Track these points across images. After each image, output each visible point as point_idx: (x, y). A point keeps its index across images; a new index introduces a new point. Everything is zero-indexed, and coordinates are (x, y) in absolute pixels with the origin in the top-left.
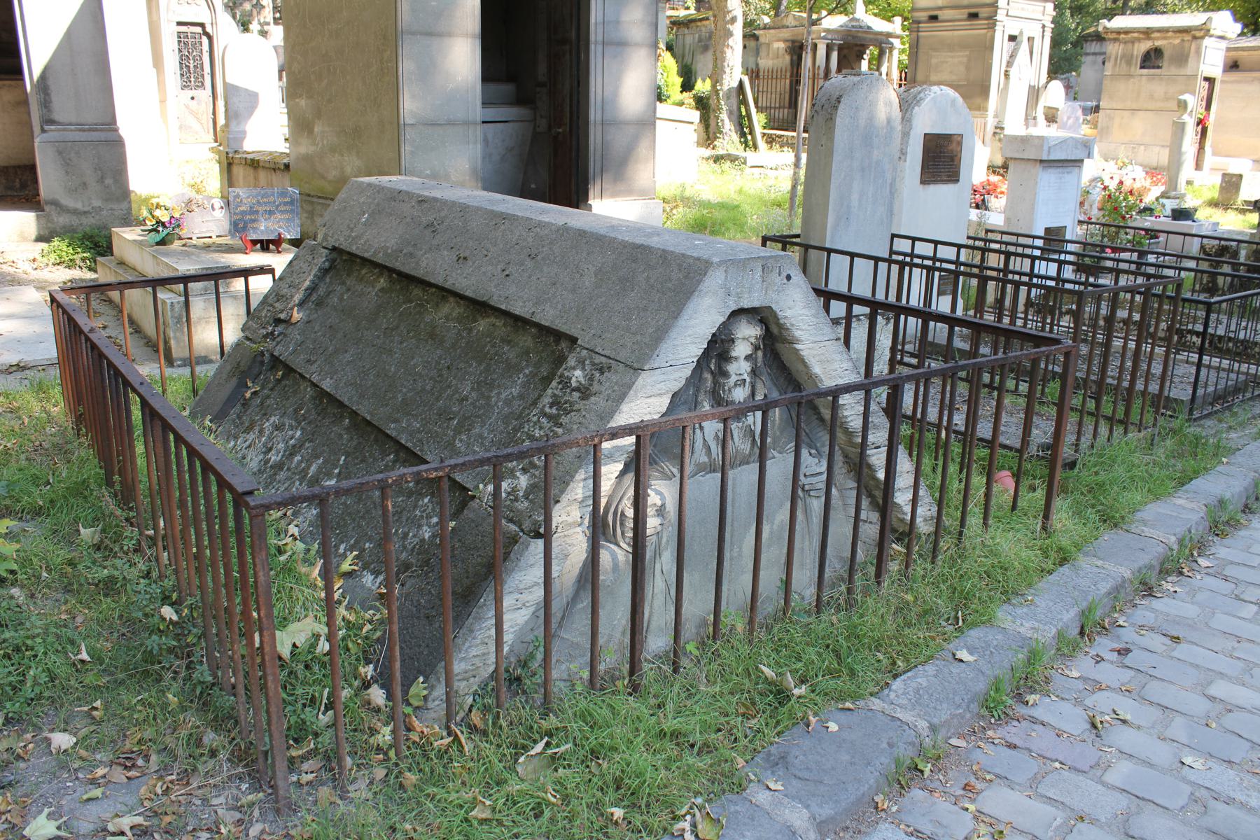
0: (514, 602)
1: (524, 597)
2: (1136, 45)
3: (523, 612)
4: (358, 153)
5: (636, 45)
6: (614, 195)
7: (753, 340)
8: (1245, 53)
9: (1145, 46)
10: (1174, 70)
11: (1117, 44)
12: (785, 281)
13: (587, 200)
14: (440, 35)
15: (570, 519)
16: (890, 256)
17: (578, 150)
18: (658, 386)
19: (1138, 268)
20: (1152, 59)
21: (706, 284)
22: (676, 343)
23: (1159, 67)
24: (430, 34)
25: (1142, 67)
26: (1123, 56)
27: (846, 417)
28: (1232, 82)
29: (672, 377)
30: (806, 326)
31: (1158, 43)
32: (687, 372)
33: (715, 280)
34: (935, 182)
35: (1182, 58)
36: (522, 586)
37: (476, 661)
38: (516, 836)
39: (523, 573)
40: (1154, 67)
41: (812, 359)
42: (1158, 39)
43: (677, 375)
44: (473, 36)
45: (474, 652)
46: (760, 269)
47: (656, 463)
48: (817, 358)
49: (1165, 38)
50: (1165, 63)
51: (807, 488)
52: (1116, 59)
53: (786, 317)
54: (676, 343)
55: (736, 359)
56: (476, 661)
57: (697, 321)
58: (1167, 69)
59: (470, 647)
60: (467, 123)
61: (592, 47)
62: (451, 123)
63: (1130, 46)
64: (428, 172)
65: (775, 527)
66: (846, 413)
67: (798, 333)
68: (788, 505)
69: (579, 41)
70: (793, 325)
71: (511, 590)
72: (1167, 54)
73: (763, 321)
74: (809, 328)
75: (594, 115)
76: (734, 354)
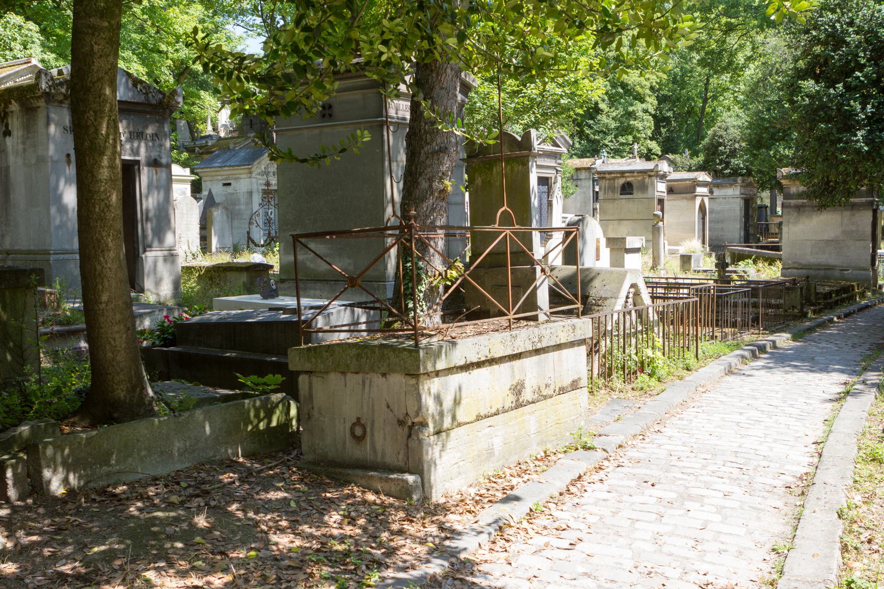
2: (616, 181)
4: (80, 310)
8: (676, 183)
9: (622, 181)
10: (640, 195)
11: (604, 181)
16: (616, 312)
19: (639, 332)
20: (627, 189)
23: (631, 194)
25: (621, 194)
26: (609, 187)
28: (672, 200)
31: (629, 179)
33: (628, 275)
34: (453, 321)
35: (644, 187)
38: (310, 587)
40: (628, 194)
42: (629, 177)
49: (633, 176)
50: (635, 192)
52: (605, 189)
58: (637, 195)
63: (612, 181)
72: (635, 186)
73: (358, 437)
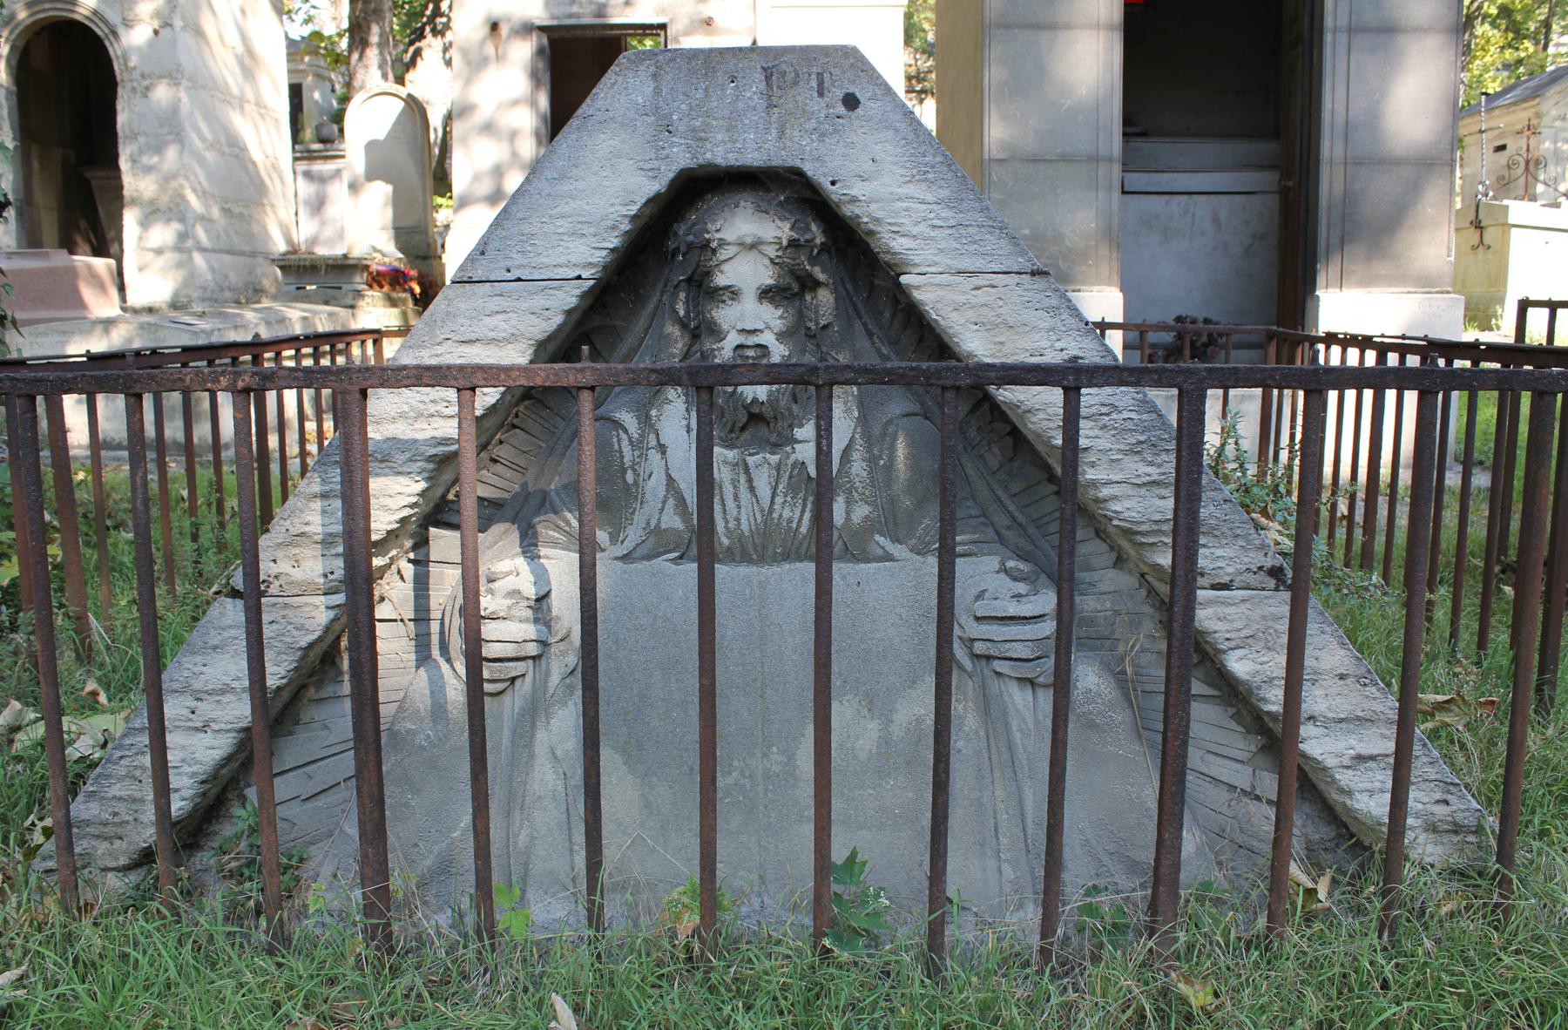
0: (186, 712)
1: (206, 709)
3: (207, 739)
5: (1418, 30)
6: (1368, 282)
7: (772, 251)
12: (841, 109)
13: (1314, 290)
14: (1053, 27)
15: (297, 574)
17: (1307, 211)
18: (487, 320)
21: (600, 103)
22: (526, 229)
24: (1038, 27)
27: (1094, 484)
29: (525, 305)
30: (921, 228)
32: (569, 297)
36: (197, 685)
37: (121, 807)
39: (198, 659)
41: (954, 316)
43: (540, 301)
44: (1110, 28)
45: (117, 790)
46: (759, 76)
47: (556, 513)
48: (970, 314)
51: (979, 648)
53: (854, 200)
54: (526, 229)
55: (734, 293)
56: (121, 807)
57: (581, 185)
59: (108, 777)
60: (1095, 159)
61: (1328, 37)
62: (1067, 159)
64: (1026, 232)
65: (897, 730)
66: (1090, 474)
67: (899, 244)
68: (930, 681)
69: (1312, 36)
70: (878, 220)
71: (176, 686)
74: (936, 233)
75: (1330, 147)
76: (721, 280)
